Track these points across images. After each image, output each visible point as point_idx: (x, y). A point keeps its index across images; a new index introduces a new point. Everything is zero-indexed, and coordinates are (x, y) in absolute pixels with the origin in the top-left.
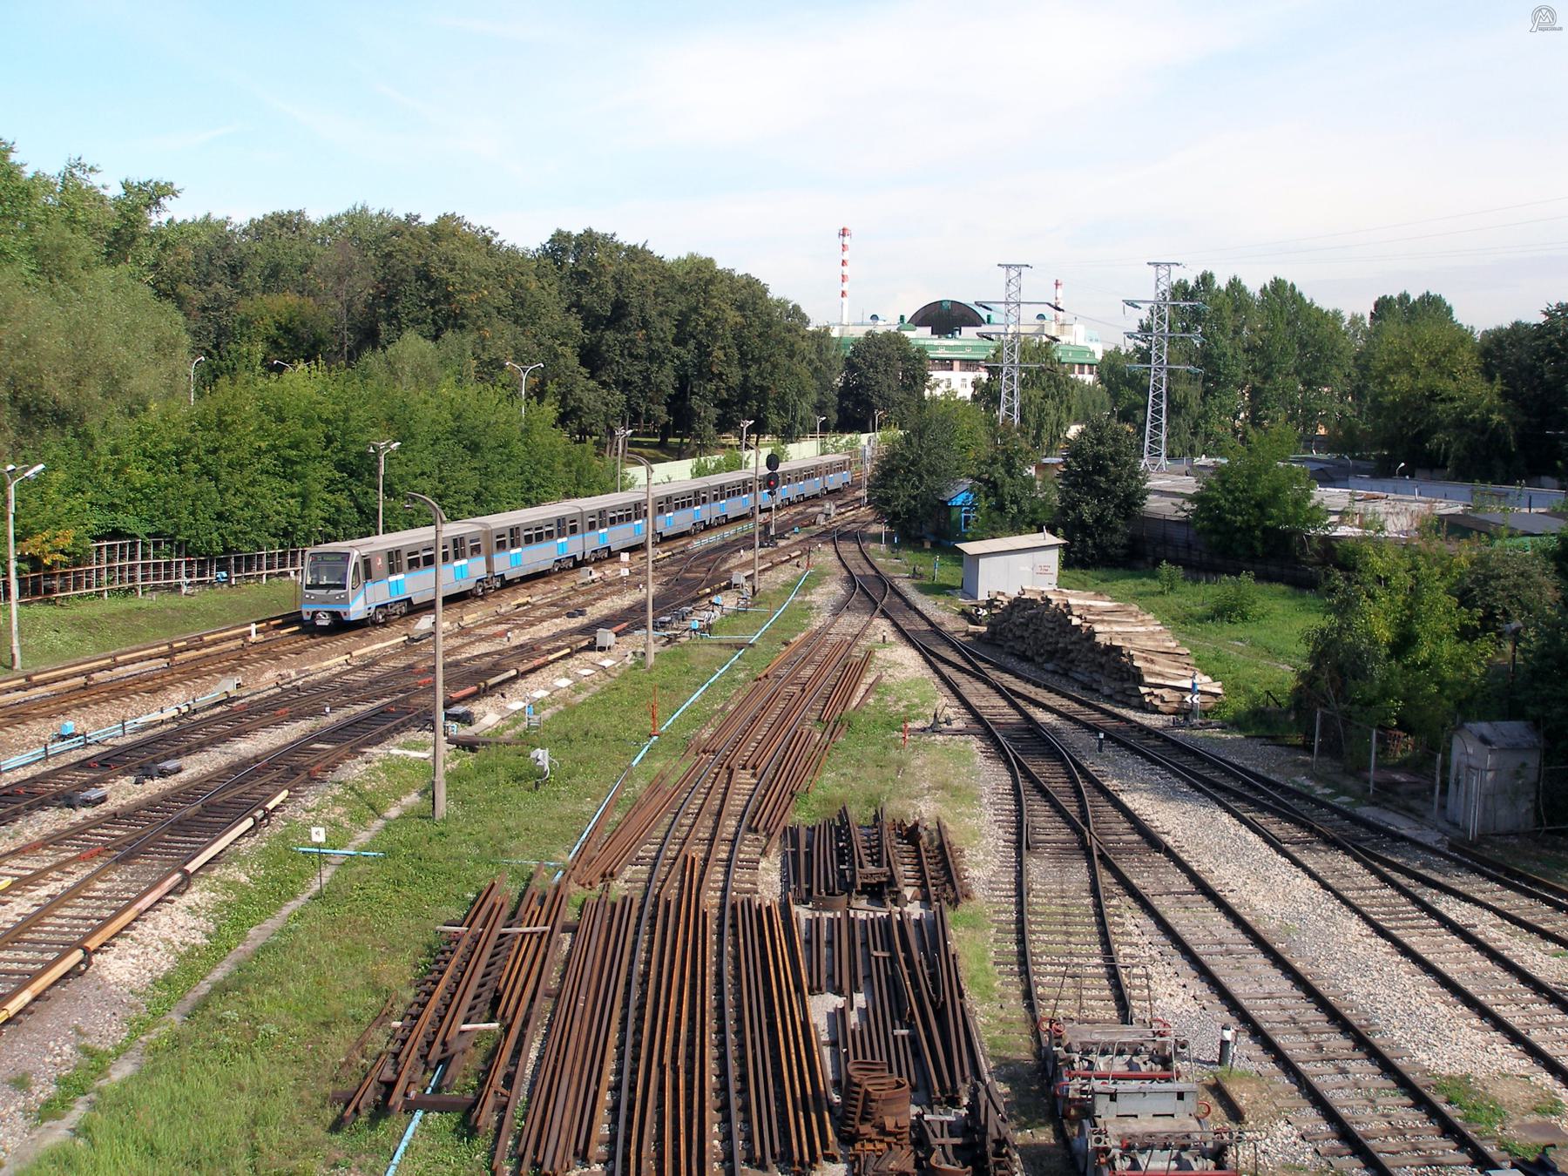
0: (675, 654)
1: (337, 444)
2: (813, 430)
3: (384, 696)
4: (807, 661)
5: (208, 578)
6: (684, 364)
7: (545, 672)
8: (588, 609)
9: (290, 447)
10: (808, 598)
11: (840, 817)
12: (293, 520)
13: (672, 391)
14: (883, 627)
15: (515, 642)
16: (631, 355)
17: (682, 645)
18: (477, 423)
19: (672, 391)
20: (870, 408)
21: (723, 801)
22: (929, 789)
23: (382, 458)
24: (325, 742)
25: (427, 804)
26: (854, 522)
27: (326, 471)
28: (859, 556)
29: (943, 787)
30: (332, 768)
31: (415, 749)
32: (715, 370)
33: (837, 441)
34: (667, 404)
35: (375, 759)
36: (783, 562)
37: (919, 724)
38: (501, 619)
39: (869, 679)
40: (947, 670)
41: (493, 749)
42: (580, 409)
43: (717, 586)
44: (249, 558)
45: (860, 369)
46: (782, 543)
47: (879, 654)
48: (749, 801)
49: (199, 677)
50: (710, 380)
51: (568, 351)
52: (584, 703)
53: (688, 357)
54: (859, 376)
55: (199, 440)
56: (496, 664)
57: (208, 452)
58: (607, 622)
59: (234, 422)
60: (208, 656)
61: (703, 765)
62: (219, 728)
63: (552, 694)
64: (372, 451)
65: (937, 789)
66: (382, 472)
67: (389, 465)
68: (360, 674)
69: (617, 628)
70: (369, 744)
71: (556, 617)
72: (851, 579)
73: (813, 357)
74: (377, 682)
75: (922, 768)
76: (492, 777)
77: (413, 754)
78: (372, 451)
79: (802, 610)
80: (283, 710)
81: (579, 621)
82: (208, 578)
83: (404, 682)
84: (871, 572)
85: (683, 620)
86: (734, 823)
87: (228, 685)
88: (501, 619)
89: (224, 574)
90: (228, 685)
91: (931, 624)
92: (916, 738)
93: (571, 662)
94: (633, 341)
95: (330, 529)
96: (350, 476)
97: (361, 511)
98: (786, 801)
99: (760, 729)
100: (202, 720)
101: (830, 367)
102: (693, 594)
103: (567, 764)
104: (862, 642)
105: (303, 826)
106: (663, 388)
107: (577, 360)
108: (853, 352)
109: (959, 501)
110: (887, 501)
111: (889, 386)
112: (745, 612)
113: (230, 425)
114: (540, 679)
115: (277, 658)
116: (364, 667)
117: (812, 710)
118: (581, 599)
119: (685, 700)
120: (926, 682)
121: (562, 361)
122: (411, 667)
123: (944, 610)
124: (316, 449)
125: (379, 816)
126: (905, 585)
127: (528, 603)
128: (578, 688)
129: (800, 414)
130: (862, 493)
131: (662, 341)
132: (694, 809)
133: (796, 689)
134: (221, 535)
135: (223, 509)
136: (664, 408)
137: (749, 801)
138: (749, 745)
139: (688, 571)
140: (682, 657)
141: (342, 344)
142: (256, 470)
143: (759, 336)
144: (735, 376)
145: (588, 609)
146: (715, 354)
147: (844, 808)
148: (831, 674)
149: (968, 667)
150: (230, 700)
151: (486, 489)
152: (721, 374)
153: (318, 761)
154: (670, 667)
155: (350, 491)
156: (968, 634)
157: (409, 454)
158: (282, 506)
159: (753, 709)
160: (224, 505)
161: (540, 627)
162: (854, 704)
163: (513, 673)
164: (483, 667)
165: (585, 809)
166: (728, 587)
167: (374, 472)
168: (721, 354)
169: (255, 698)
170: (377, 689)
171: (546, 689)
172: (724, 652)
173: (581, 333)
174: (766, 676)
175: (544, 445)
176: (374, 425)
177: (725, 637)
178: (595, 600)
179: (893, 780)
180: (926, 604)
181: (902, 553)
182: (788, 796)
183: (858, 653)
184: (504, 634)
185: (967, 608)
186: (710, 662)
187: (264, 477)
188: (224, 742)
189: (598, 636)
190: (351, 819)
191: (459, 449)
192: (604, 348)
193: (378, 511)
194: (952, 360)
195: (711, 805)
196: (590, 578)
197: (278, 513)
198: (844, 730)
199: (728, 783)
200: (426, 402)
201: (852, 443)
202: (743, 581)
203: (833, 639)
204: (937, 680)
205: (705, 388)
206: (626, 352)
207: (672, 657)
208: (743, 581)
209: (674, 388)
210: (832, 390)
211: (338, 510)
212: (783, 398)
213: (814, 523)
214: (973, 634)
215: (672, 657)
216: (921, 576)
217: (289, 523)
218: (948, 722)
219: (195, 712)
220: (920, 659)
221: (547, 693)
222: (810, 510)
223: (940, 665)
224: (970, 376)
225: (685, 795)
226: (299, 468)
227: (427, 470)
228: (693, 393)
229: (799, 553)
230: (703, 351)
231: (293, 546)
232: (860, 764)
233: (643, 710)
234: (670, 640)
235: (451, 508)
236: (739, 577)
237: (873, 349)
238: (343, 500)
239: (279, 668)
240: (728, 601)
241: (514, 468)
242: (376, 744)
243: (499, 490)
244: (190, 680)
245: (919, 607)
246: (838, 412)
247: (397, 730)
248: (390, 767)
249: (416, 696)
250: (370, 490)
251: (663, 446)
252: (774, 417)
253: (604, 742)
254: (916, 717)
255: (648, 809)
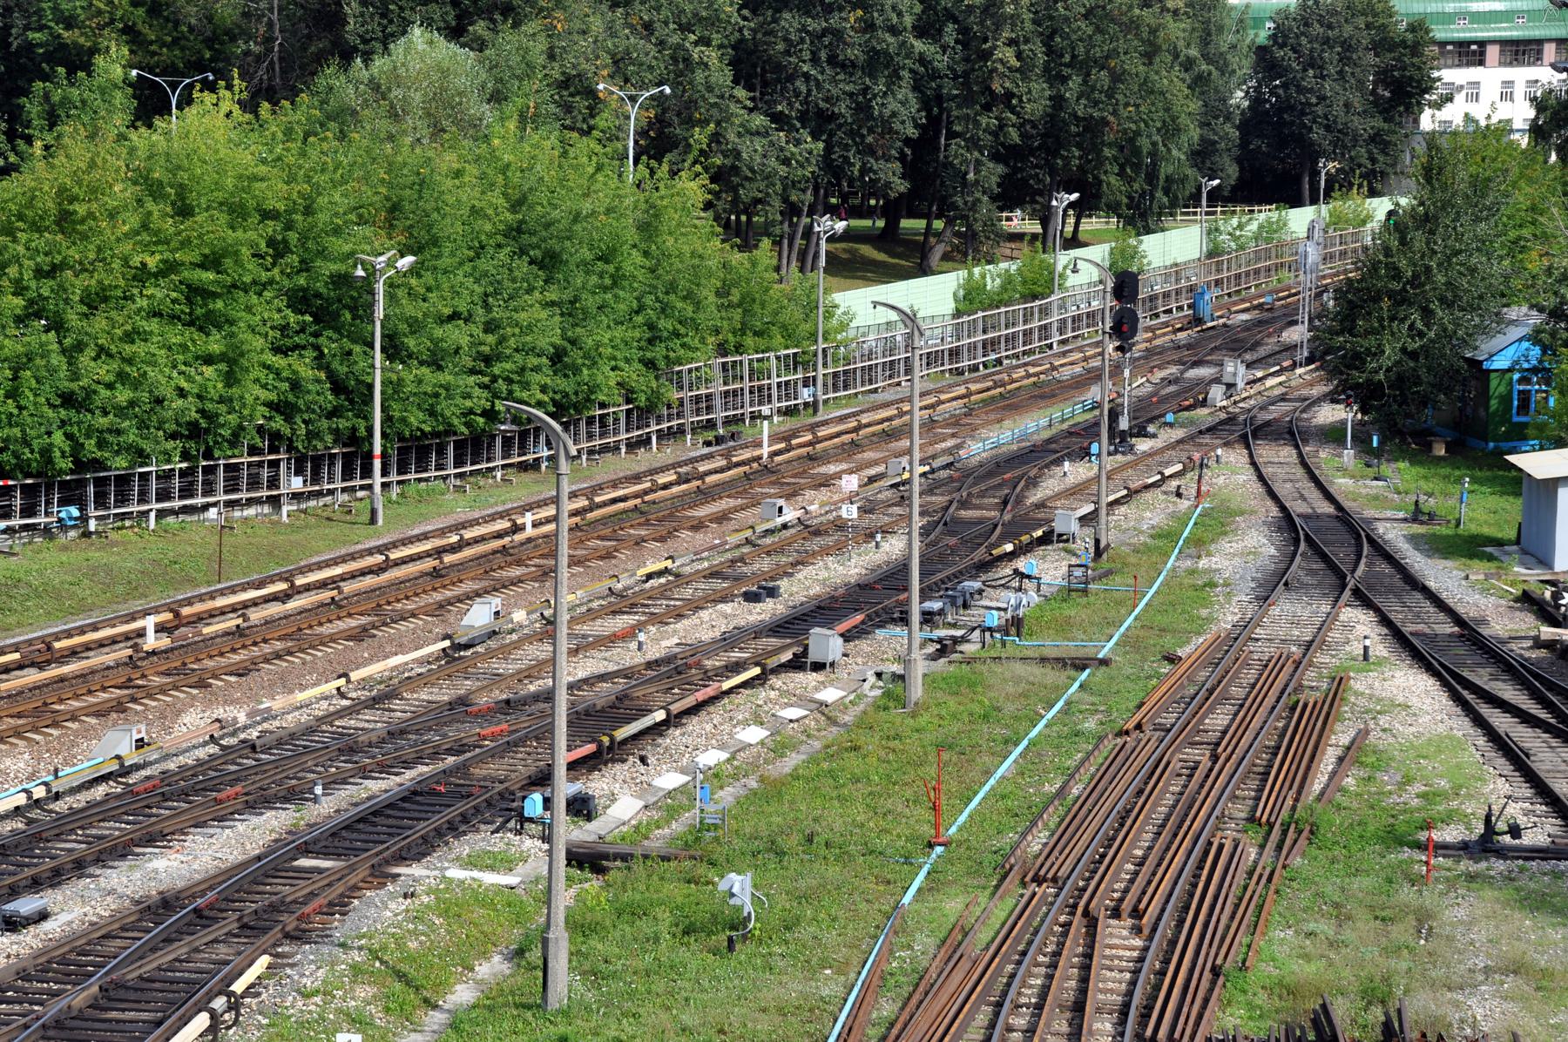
0: (959, 681)
1: (293, 259)
2: (1195, 199)
3: (419, 760)
4: (1210, 695)
5: (41, 520)
6: (935, 75)
7: (716, 713)
8: (783, 584)
9: (203, 266)
10: (1203, 563)
11: (1316, 1023)
12: (209, 406)
13: (912, 132)
14: (1359, 626)
15: (654, 652)
16: (832, 60)
17: (969, 661)
18: (556, 214)
19: (912, 132)
20: (1312, 155)
21: (1084, 980)
22: (1487, 970)
23: (380, 288)
24: (318, 854)
25: (528, 982)
26: (1283, 398)
27: (270, 311)
28: (1300, 472)
29: (1516, 969)
30: (340, 906)
31: (492, 868)
32: (997, 87)
33: (1240, 226)
34: (902, 158)
35: (419, 889)
36: (1147, 487)
37: (1450, 834)
38: (621, 603)
39: (1341, 736)
40: (1501, 722)
41: (638, 868)
42: (735, 170)
43: (1025, 539)
44: (123, 481)
45: (1288, 69)
46: (1143, 445)
47: (1358, 684)
48: (1133, 983)
49: (55, 725)
50: (987, 108)
51: (712, 56)
52: (795, 776)
53: (942, 61)
54: (1285, 86)
55: (21, 249)
56: (622, 698)
57: (39, 273)
58: (824, 611)
59: (91, 215)
60: (62, 679)
61: (1038, 907)
62: (111, 829)
63: (733, 757)
64: (360, 272)
65: (1506, 971)
66: (380, 312)
67: (391, 298)
68: (368, 715)
69: (845, 625)
70: (402, 858)
71: (724, 600)
72: (1287, 523)
73: (1194, 52)
74: (403, 732)
75: (1469, 924)
76: (645, 926)
77: (490, 878)
78: (360, 272)
79: (1195, 588)
80: (230, 791)
81: (766, 611)
82: (41, 520)
83: (453, 733)
84: (1326, 508)
85: (965, 606)
86: (1108, 1026)
87: (118, 742)
88: (621, 603)
89: (75, 512)
90: (118, 742)
91: (1458, 620)
92: (1449, 863)
93: (762, 694)
94: (838, 34)
95: (278, 423)
96: (317, 319)
97: (338, 387)
98: (1205, 984)
99: (1137, 838)
100: (73, 812)
101: (1224, 69)
102: (980, 554)
103: (783, 901)
104: (1321, 658)
105: (301, 1024)
106: (897, 126)
107: (729, 74)
108: (1273, 37)
109: (1501, 363)
110: (1356, 360)
111: (1347, 105)
112: (1085, 591)
113: (82, 221)
114: (709, 727)
115: (202, 684)
116: (373, 703)
117: (1234, 798)
118: (765, 564)
119: (988, 773)
120: (1458, 745)
121: (699, 76)
122: (463, 701)
123: (1485, 591)
124: (252, 271)
125: (435, 1007)
126: (1394, 534)
127: (666, 571)
128: (779, 746)
129: (1165, 169)
130: (1297, 334)
131: (893, 30)
132: (1029, 996)
133: (1201, 755)
134: (69, 436)
135: (74, 386)
136: (897, 166)
137: (1133, 983)
138: (1120, 869)
139: (964, 504)
140: (972, 685)
141: (269, 40)
142: (140, 310)
143: (1085, 17)
144: (1036, 98)
145: (783, 584)
146: (998, 54)
147: (1324, 1006)
148: (1267, 726)
149: (1543, 715)
150: (125, 771)
151: (573, 342)
152: (1009, 95)
153: (312, 895)
154: (952, 703)
155: (317, 348)
156: (1538, 643)
157: (428, 278)
158: (189, 379)
159: (1118, 794)
160: (75, 377)
161: (694, 620)
162: (1317, 787)
163: (660, 715)
164: (600, 703)
165: (825, 992)
166: (1045, 540)
167: (363, 310)
168: (1009, 54)
169: (172, 765)
170: (406, 747)
171: (722, 747)
172: (1051, 676)
173: (735, 18)
174: (1139, 727)
175: (680, 255)
176: (362, 221)
177: (1053, 645)
178: (793, 565)
179: (1411, 950)
180: (1443, 576)
181: (1386, 469)
182: (1207, 975)
183: (1314, 681)
184: (629, 634)
185: (1534, 588)
186: (1024, 695)
187: (153, 325)
188: (123, 856)
189: (811, 642)
190: (387, 1010)
191: (522, 267)
192: (781, 47)
193: (371, 387)
194: (1482, 44)
195: (1061, 989)
196: (780, 521)
197: (182, 393)
198: (1302, 842)
199: (1091, 945)
200: (458, 174)
201: (1268, 231)
202: (1074, 527)
203: (1262, 650)
204: (1482, 741)
205: (977, 124)
206: (823, 55)
207: (954, 686)
208: (1074, 527)
209: (916, 126)
210: (1228, 117)
211: (295, 385)
212: (1132, 140)
213: (1204, 403)
214: (1550, 645)
215: (954, 686)
216: (1431, 517)
217: (202, 412)
218: (1515, 831)
219: (57, 796)
220: (1443, 698)
221: (724, 756)
222: (1193, 373)
223: (1486, 710)
224: (1522, 75)
225: (1009, 968)
226: (219, 304)
227: (463, 308)
228: (952, 135)
229: (1179, 467)
230: (974, 48)
231: (208, 455)
232: (1341, 916)
233: (909, 793)
234: (944, 649)
235: (509, 381)
236: (1067, 520)
237: (1317, 29)
238: (303, 367)
239: (208, 704)
240: (1049, 568)
241: (625, 301)
242: (419, 857)
243: (598, 345)
244: (36, 730)
245: (1432, 584)
246: (1239, 161)
247: (455, 829)
248: (453, 904)
249: (479, 760)
250: (357, 349)
251: (888, 238)
252: (1113, 179)
253: (844, 857)
254: (1447, 819)
255: (944, 997)
